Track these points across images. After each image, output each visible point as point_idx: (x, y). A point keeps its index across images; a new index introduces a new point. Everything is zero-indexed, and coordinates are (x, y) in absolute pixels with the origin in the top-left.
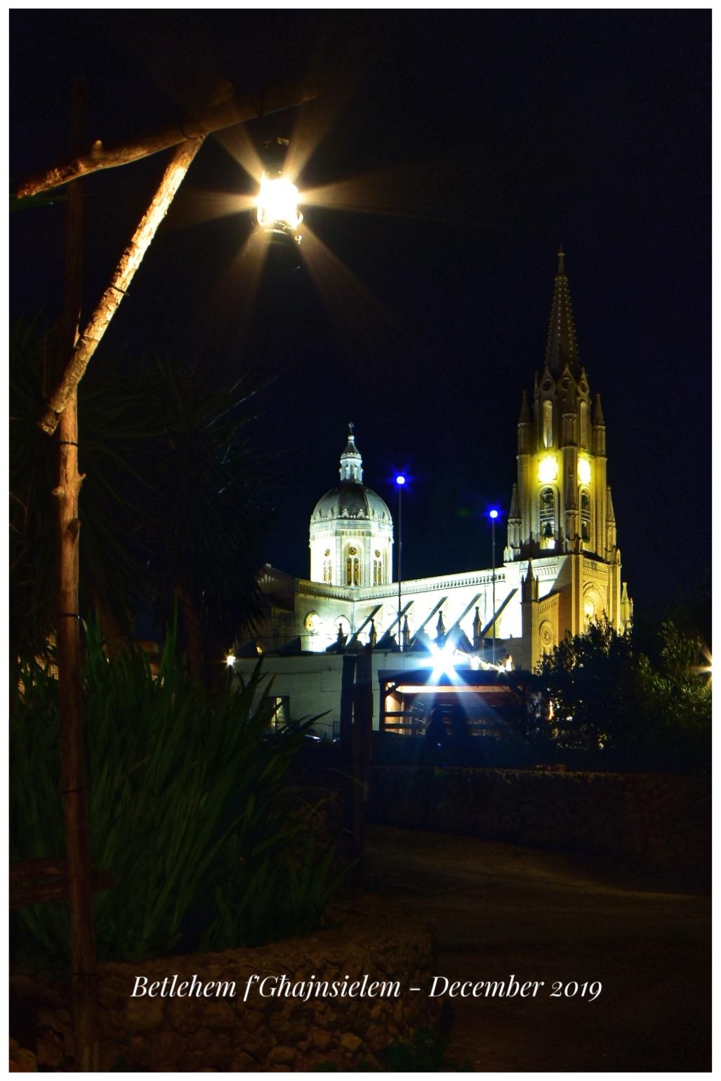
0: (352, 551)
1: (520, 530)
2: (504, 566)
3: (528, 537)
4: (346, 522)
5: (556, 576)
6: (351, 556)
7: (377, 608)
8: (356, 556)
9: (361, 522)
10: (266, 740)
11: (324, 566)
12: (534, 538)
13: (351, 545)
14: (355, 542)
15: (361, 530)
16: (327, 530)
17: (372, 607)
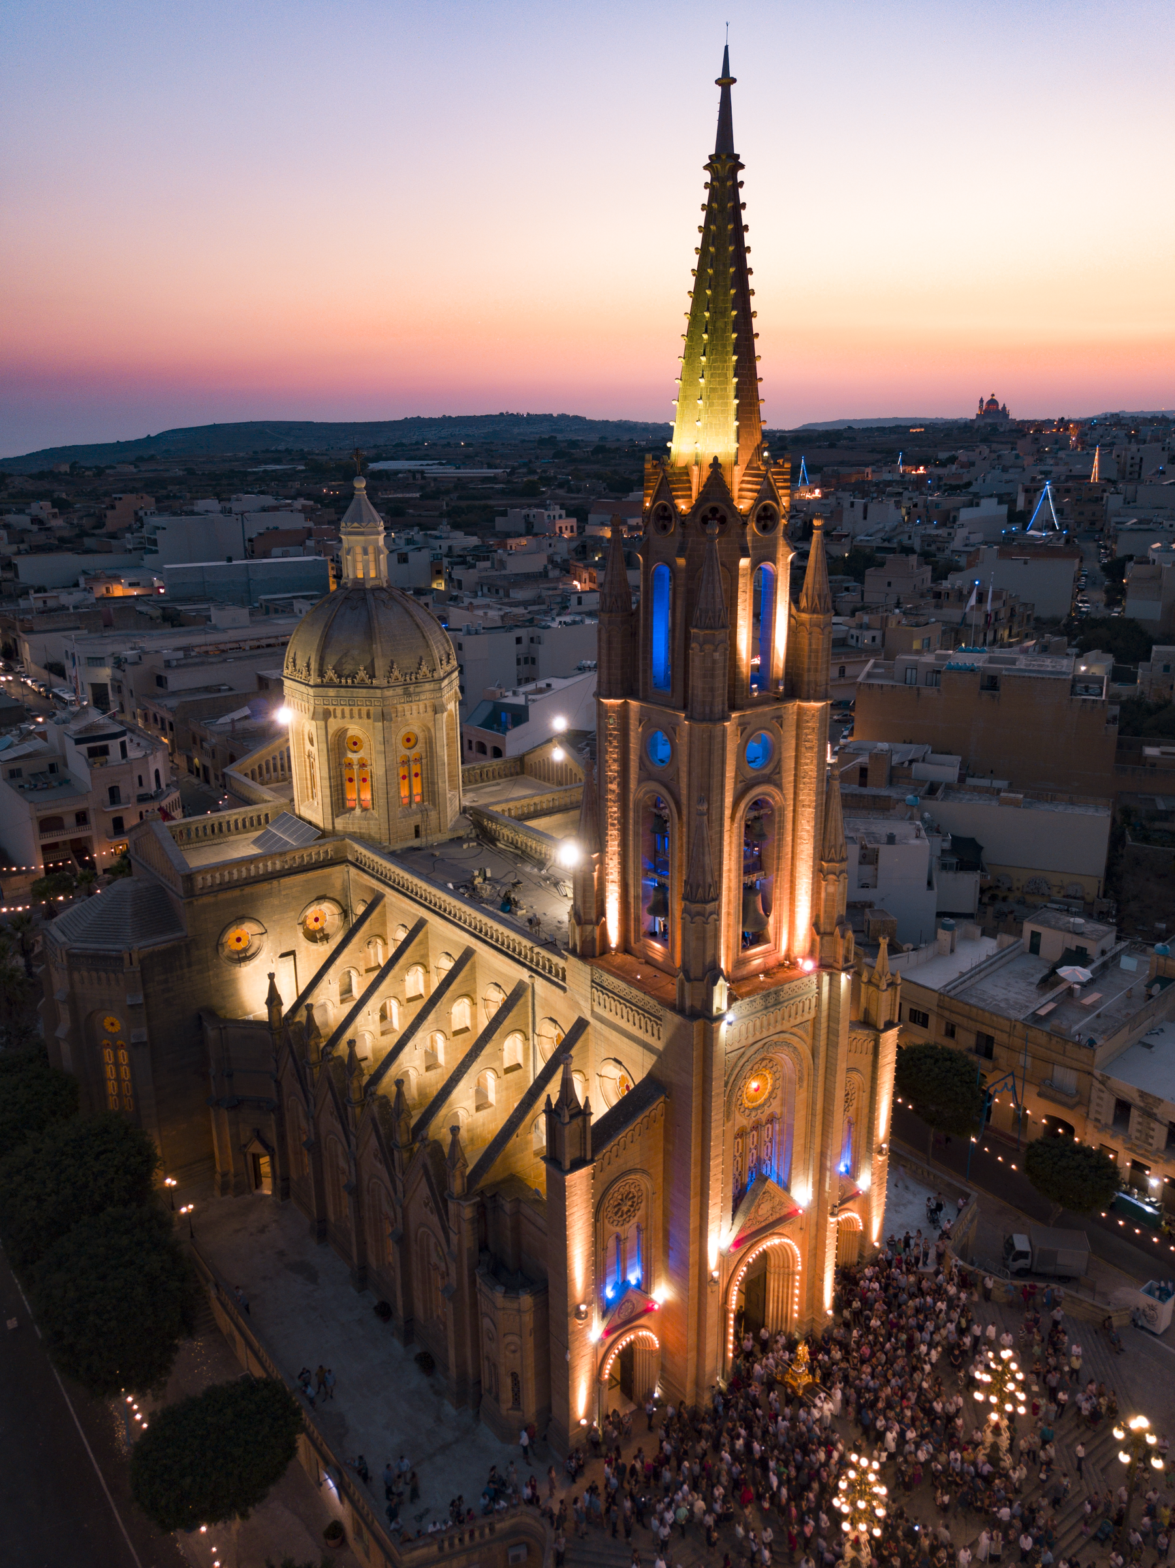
4: (332, 692)
8: (361, 754)
14: (355, 729)
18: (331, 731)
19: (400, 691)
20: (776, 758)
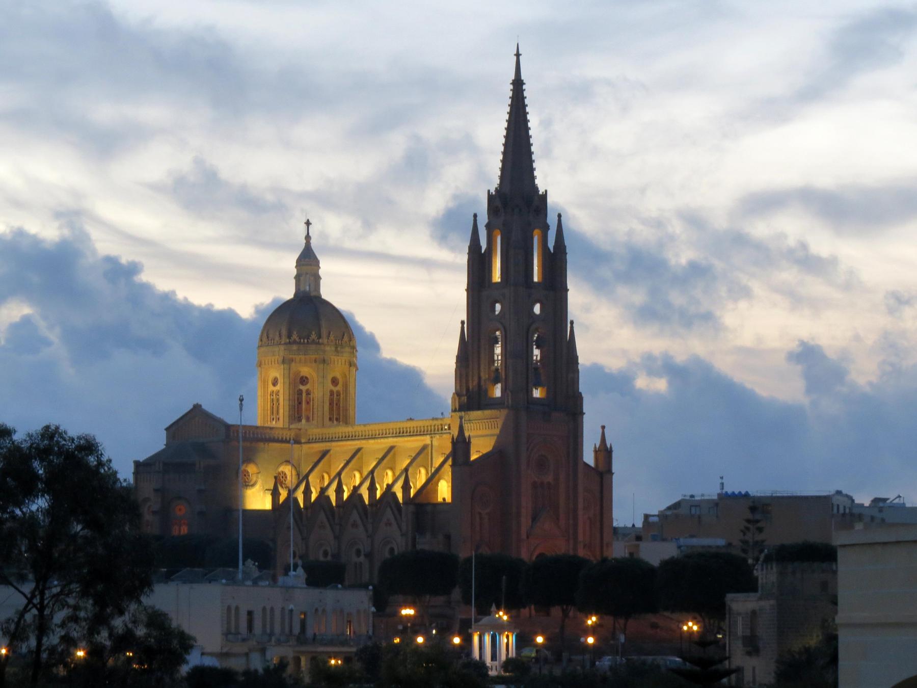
0: (304, 380)
1: (467, 376)
2: (611, 447)
3: (475, 383)
4: (295, 347)
5: (497, 431)
6: (301, 387)
7: (325, 454)
8: (308, 386)
9: (313, 347)
10: (108, 610)
11: (720, 481)
12: (482, 383)
13: (302, 374)
14: (305, 371)
15: (313, 357)
16: (274, 355)
17: (320, 452)
18: (292, 372)
19: (333, 349)
20: (552, 220)
